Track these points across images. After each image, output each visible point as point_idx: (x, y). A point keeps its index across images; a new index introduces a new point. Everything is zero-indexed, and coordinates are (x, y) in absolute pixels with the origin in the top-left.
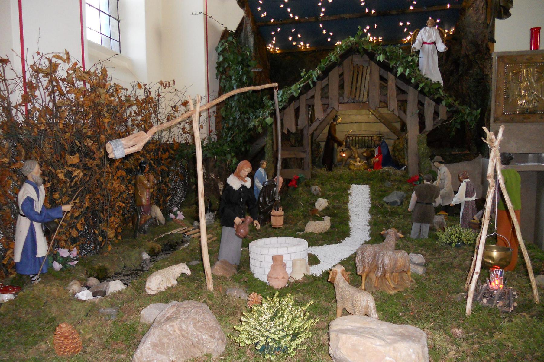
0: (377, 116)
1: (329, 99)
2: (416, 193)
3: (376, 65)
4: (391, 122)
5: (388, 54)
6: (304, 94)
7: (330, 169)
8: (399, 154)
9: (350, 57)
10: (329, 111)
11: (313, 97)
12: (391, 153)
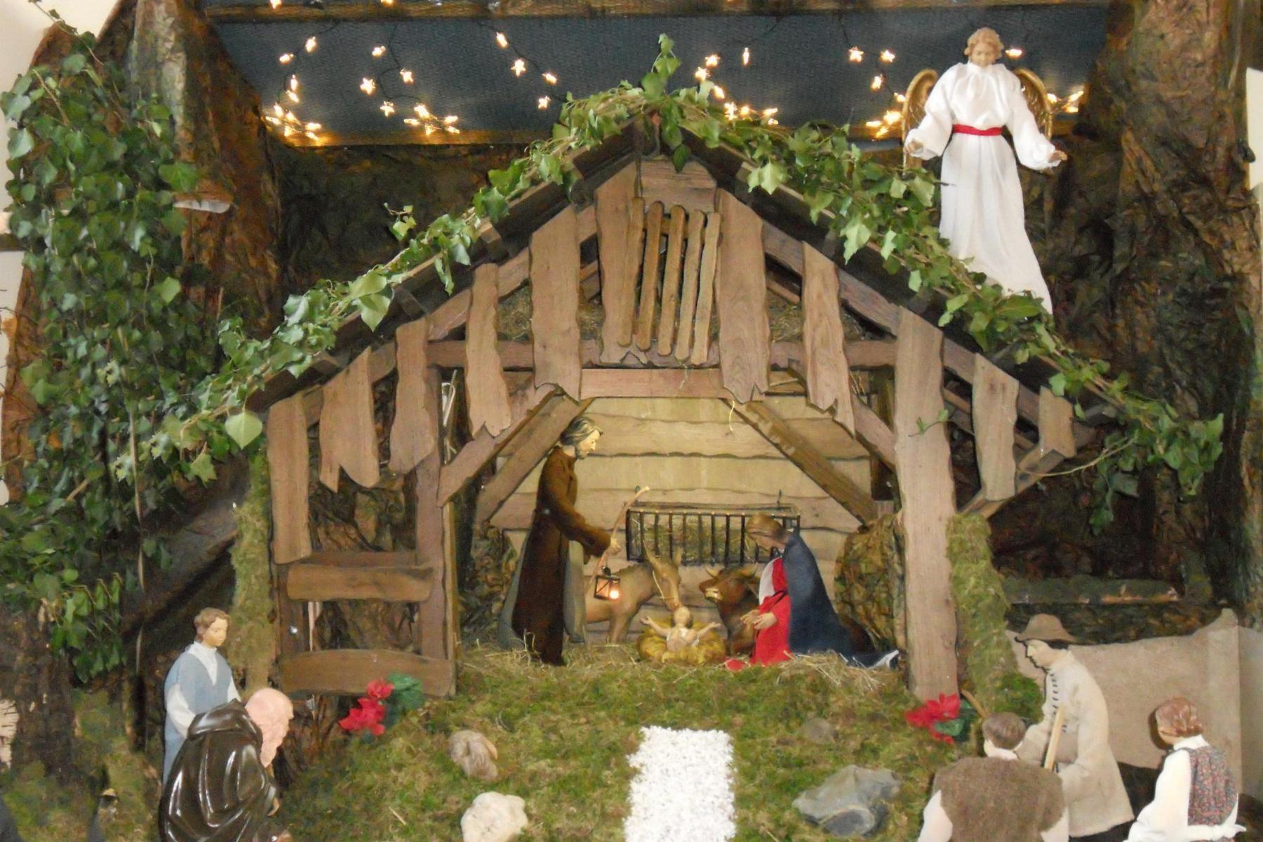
0: (765, 428)
1: (537, 345)
2: (944, 804)
3: (747, 210)
4: (829, 459)
5: (799, 163)
6: (409, 319)
7: (550, 653)
8: (870, 598)
9: (629, 171)
10: (535, 397)
11: (460, 334)
12: (831, 595)
